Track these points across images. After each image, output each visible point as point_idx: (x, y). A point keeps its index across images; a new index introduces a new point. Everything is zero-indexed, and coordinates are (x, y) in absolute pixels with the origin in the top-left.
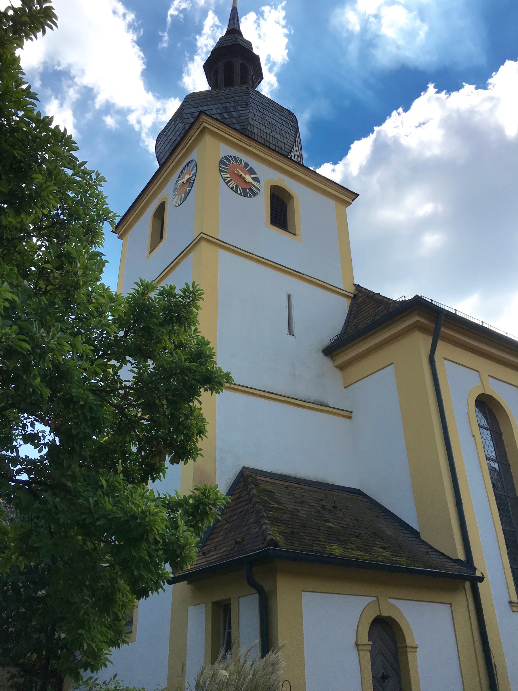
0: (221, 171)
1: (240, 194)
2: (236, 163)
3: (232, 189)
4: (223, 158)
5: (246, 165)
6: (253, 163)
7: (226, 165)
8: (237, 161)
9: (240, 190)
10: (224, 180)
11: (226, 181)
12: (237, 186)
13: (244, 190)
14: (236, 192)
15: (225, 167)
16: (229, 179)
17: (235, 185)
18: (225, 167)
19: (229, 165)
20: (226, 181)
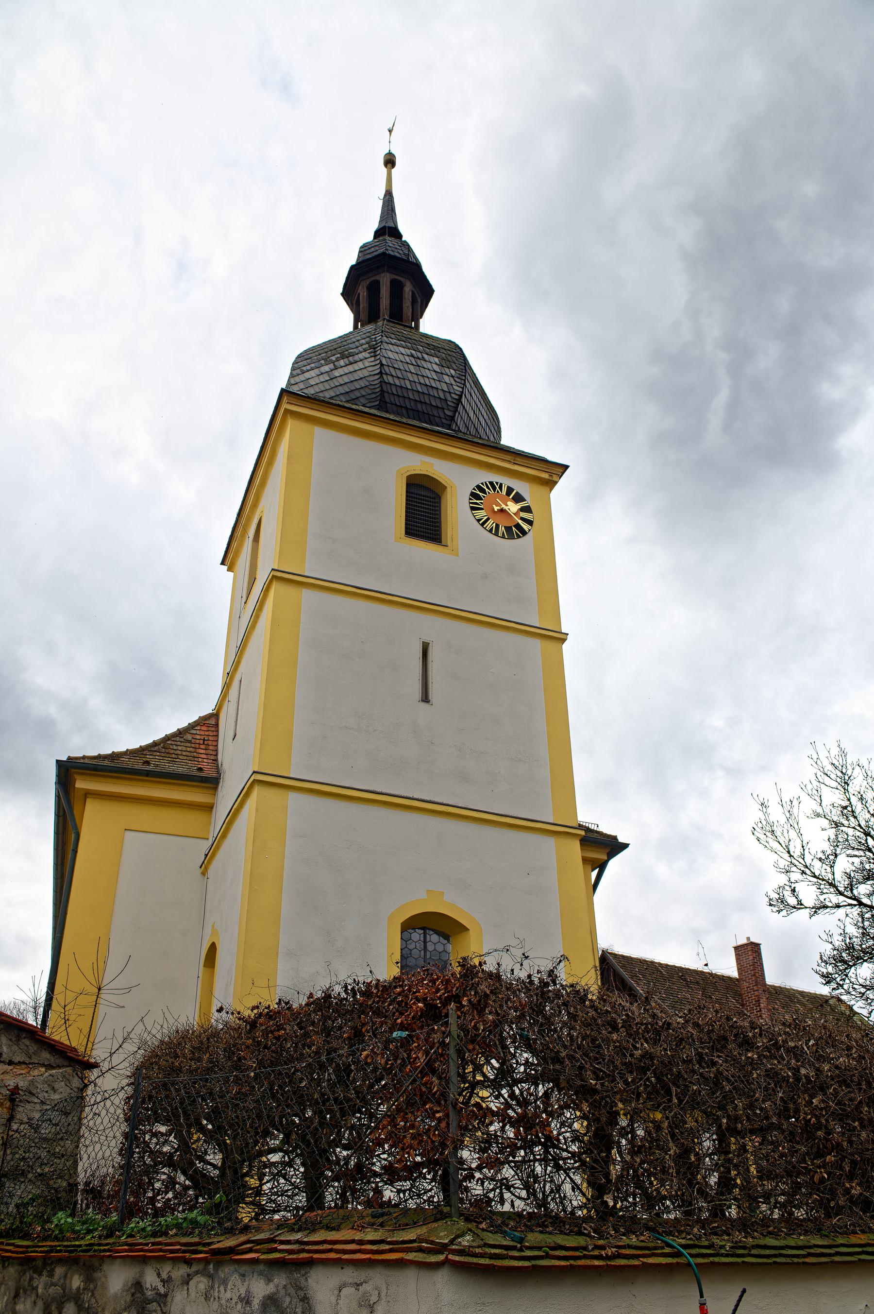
0: (473, 509)
1: (503, 537)
2: (495, 491)
3: (490, 531)
4: (474, 489)
5: (510, 490)
6: (520, 487)
7: (478, 497)
8: (494, 489)
9: (502, 529)
10: (479, 520)
11: (481, 522)
12: (497, 526)
13: (508, 529)
14: (496, 534)
15: (478, 501)
16: (486, 518)
17: (494, 524)
18: (478, 501)
19: (484, 497)
20: (481, 522)
